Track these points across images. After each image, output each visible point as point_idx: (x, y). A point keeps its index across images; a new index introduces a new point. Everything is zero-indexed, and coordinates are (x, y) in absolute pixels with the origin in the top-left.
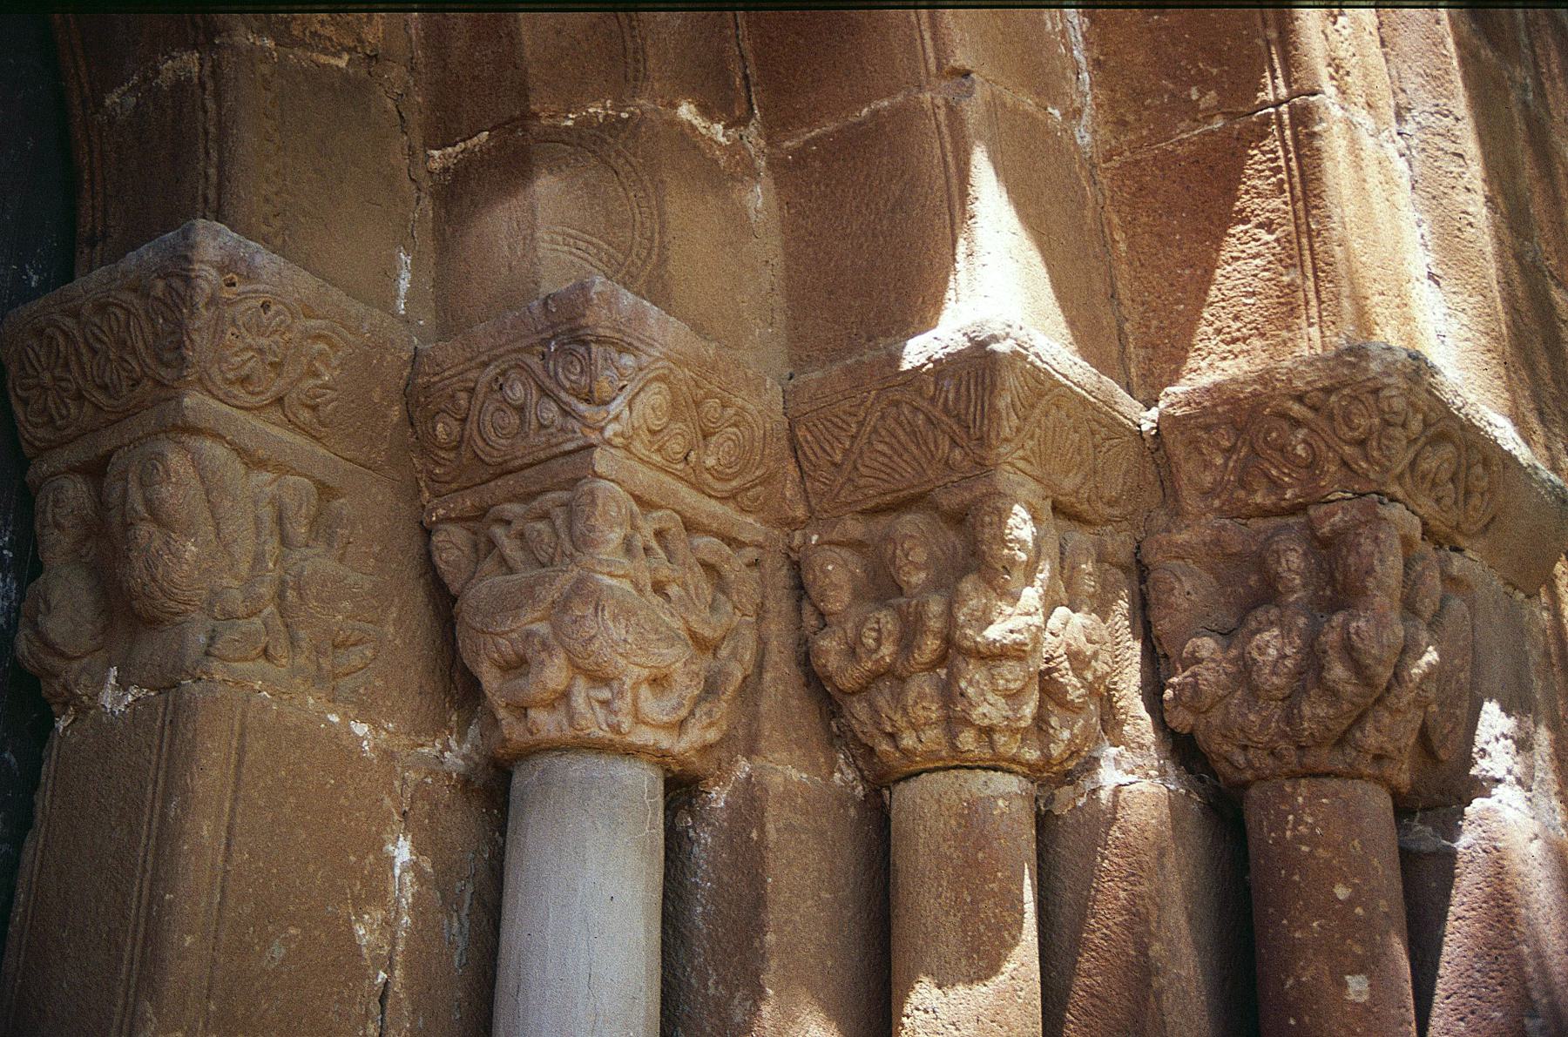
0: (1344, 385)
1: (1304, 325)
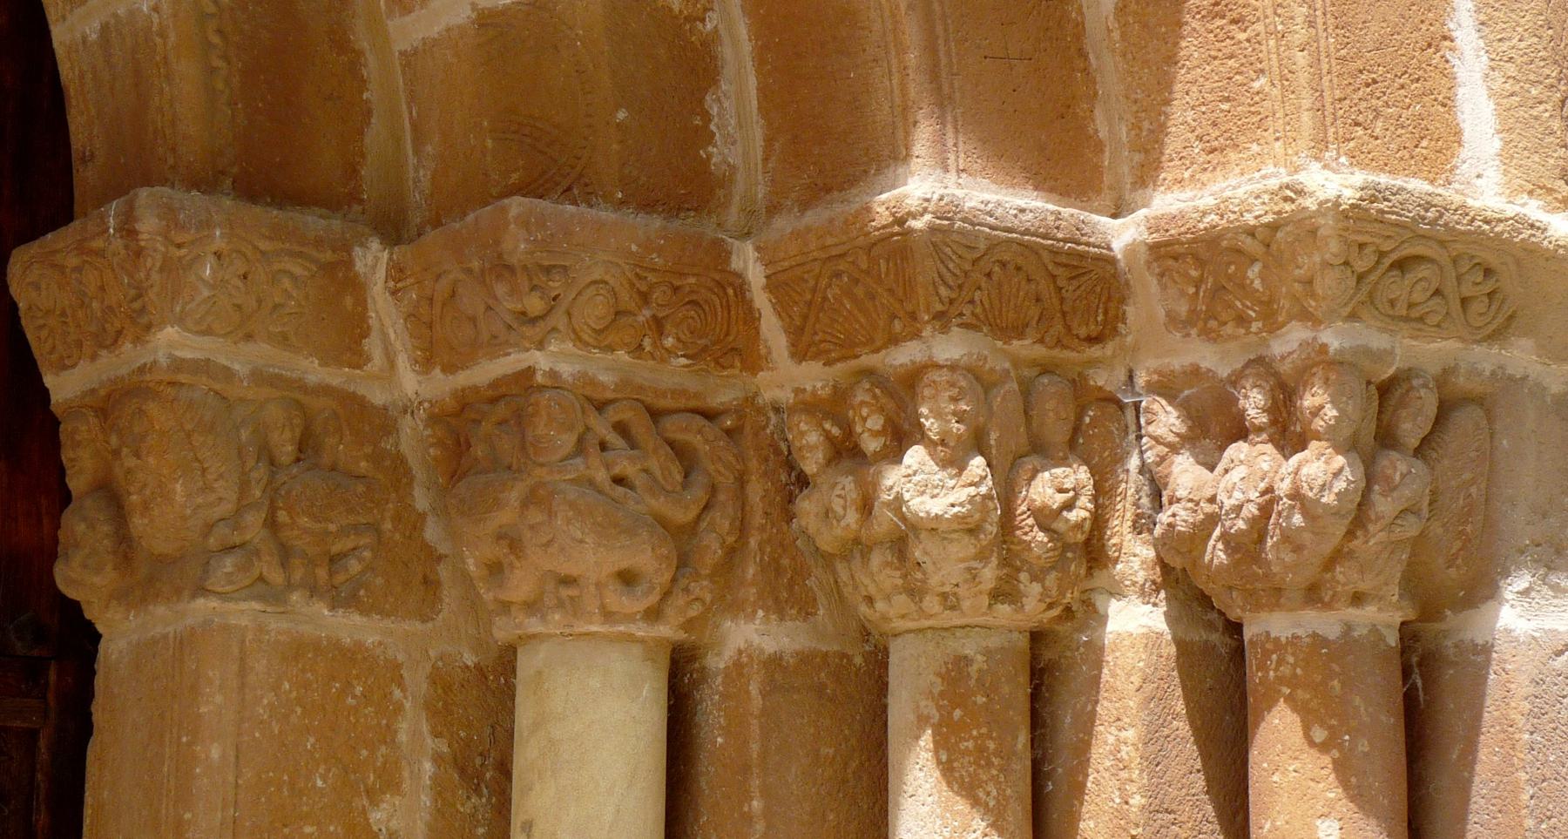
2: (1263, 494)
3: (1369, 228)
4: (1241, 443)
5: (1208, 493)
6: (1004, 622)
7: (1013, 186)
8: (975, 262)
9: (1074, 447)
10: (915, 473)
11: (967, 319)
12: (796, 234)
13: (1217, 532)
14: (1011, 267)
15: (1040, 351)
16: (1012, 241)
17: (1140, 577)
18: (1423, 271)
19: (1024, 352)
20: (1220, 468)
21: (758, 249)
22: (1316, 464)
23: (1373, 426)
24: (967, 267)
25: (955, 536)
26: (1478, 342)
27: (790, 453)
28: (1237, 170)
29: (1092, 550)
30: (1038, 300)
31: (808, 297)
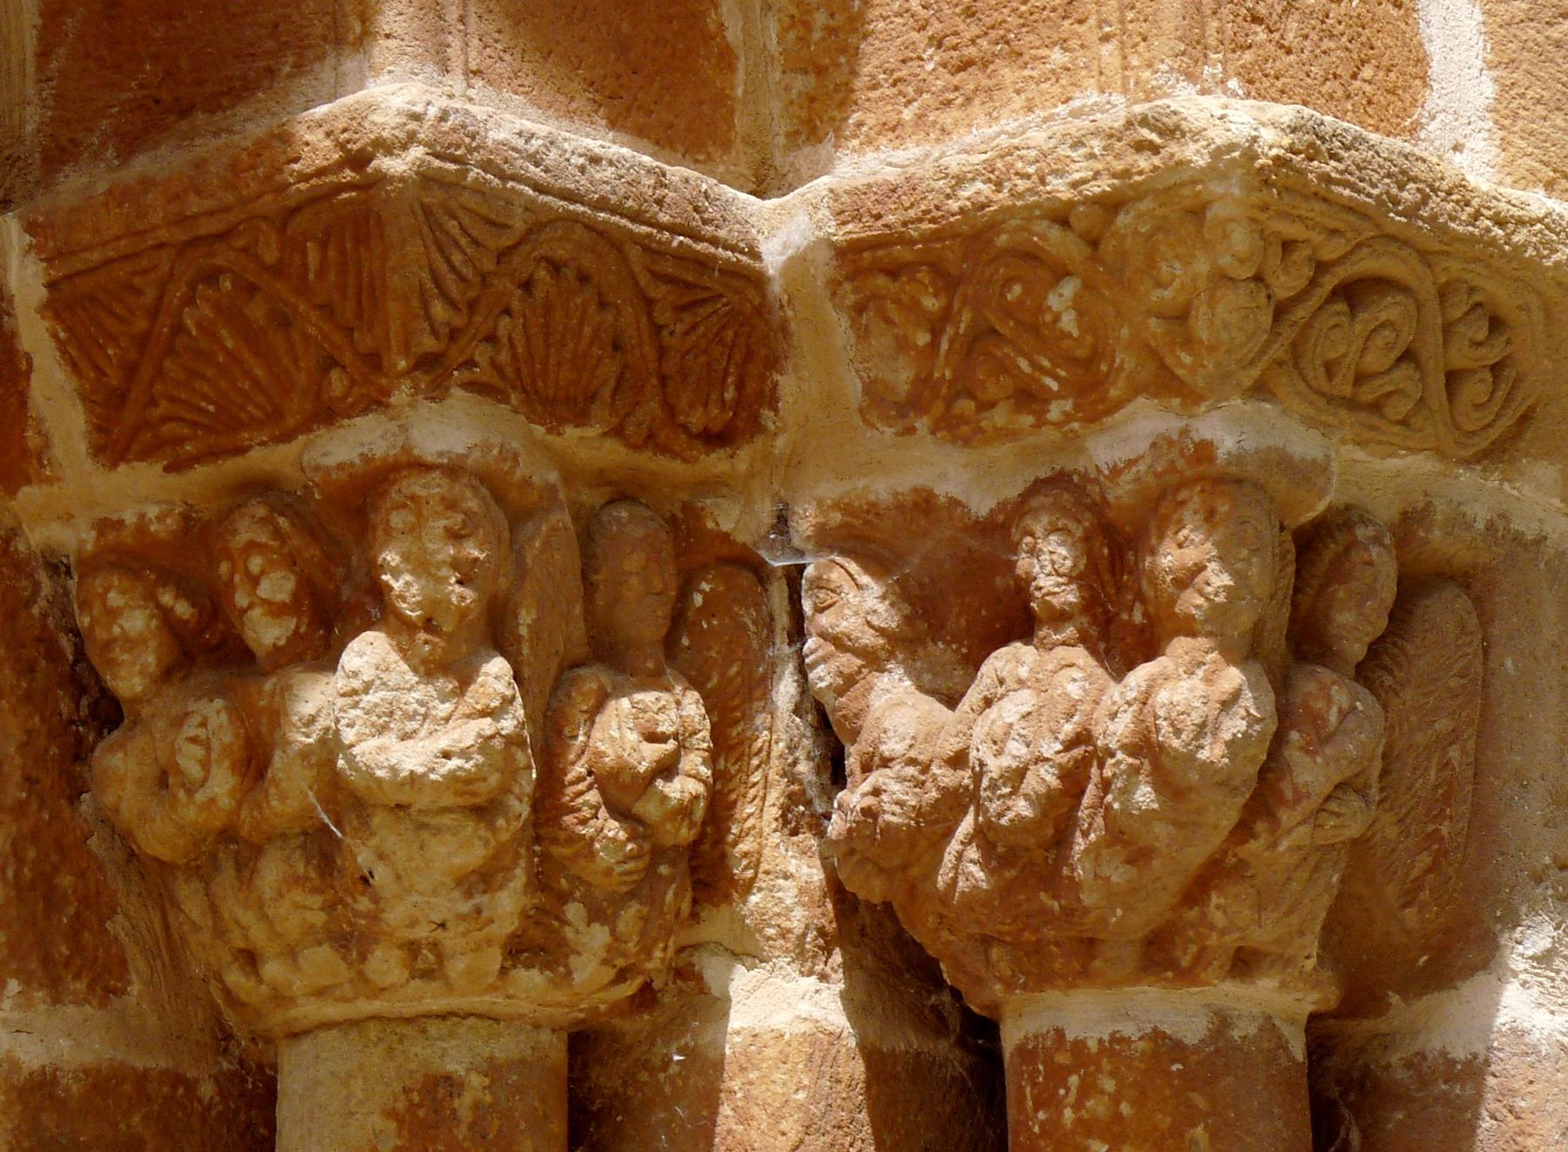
2: (1069, 745)
3: (1304, 208)
4: (1017, 647)
5: (951, 746)
6: (525, 1007)
7: (570, 115)
8: (502, 256)
9: (673, 654)
10: (367, 687)
11: (482, 373)
12: (120, 195)
13: (967, 825)
14: (569, 273)
15: (613, 454)
16: (574, 218)
17: (798, 919)
18: (1390, 309)
19: (583, 454)
20: (973, 697)
21: (31, 227)
22: (1185, 684)
23: (1286, 613)
24: (488, 264)
25: (446, 820)
26: (1466, 463)
27: (80, 653)
28: (1019, 102)
29: (701, 865)
30: (617, 347)
31: (141, 324)
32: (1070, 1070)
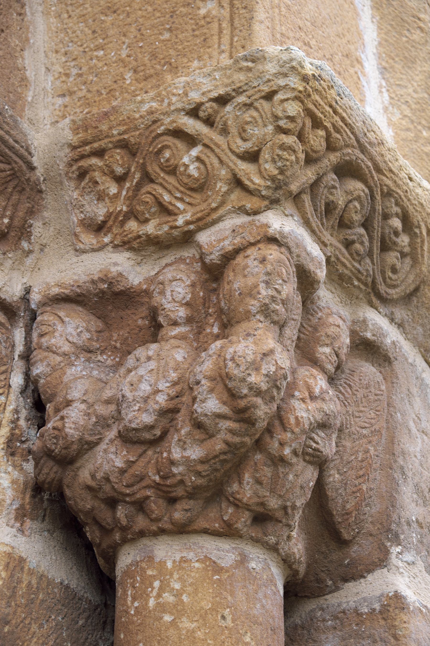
0: (239, 91)
1: (215, 53)
32: (154, 577)
